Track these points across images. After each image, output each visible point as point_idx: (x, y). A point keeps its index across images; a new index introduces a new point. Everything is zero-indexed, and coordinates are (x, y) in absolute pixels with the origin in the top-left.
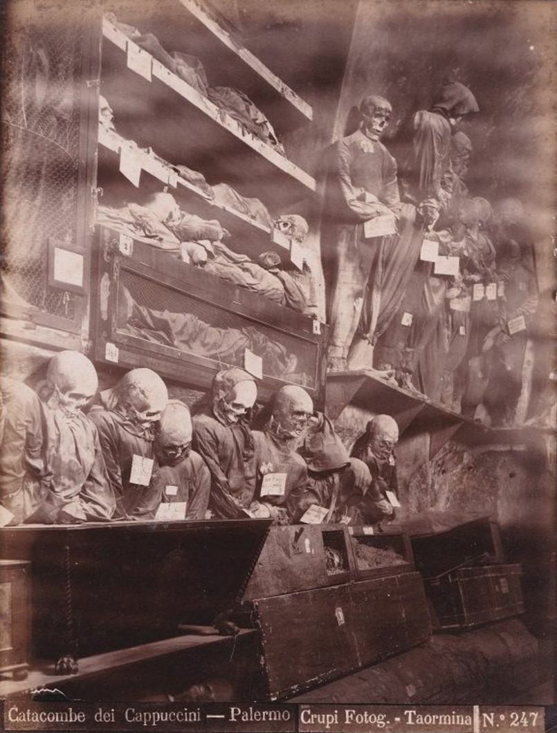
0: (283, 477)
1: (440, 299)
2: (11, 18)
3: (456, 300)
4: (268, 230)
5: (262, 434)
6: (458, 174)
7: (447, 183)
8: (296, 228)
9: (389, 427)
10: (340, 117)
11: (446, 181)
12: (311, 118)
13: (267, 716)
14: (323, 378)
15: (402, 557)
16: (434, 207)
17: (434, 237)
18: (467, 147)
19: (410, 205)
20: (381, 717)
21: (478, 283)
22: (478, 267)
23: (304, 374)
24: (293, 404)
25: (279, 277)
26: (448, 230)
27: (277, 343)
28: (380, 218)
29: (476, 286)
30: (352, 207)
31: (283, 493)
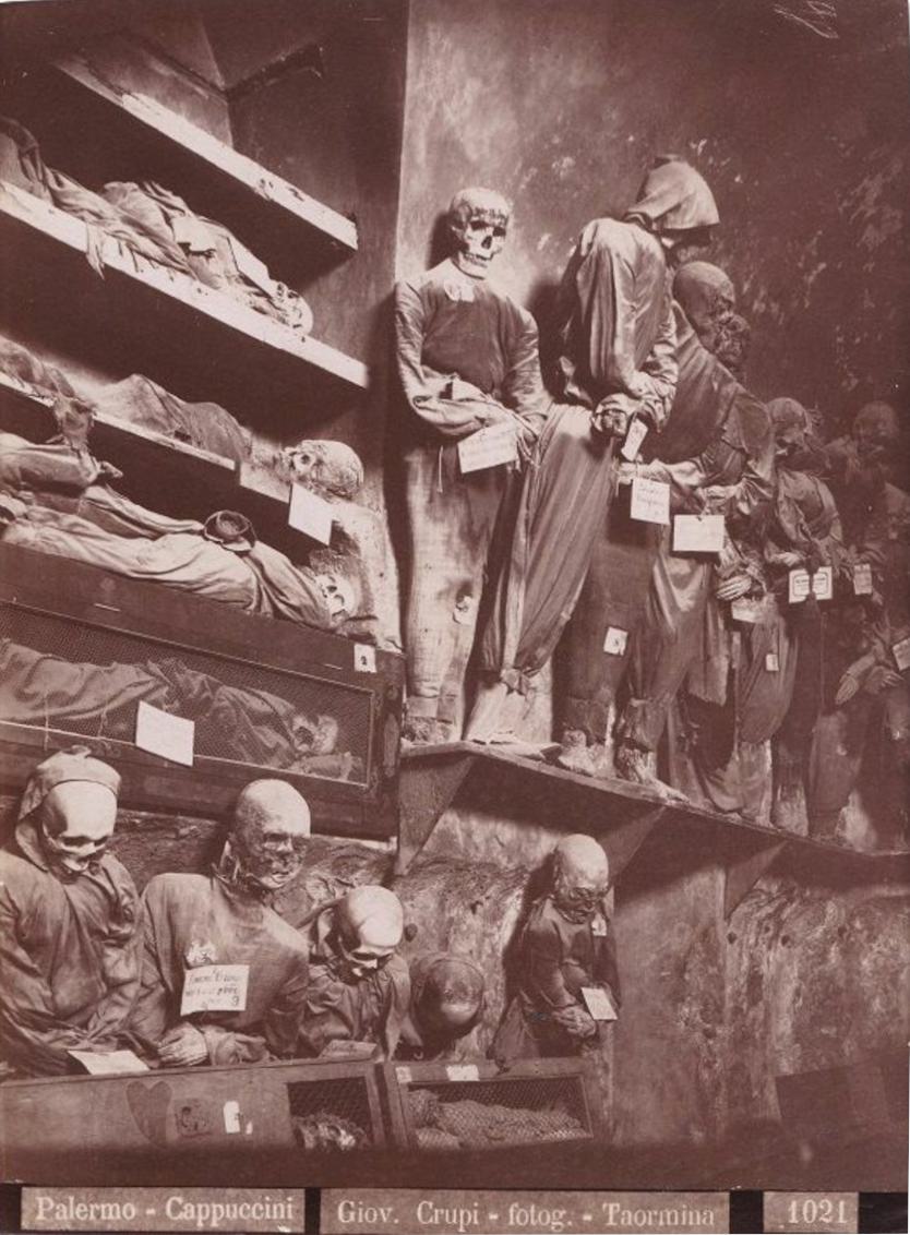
0: (240, 973)
1: (691, 599)
2: (422, 649)
3: (745, 602)
4: (230, 464)
5: (207, 881)
6: (712, 351)
7: (666, 367)
8: (324, 468)
9: (589, 859)
10: (407, 231)
11: (661, 362)
12: (355, 246)
13: (98, 1215)
14: (390, 760)
15: (577, 1122)
16: (620, 411)
17: (659, 473)
18: (725, 294)
19: (580, 409)
20: (557, 1214)
21: (795, 567)
22: (794, 537)
23: (347, 754)
24: (261, 819)
25: (250, 558)
26: (695, 463)
27: (258, 692)
28: (487, 430)
29: (793, 574)
30: (421, 412)
31: (241, 1007)
